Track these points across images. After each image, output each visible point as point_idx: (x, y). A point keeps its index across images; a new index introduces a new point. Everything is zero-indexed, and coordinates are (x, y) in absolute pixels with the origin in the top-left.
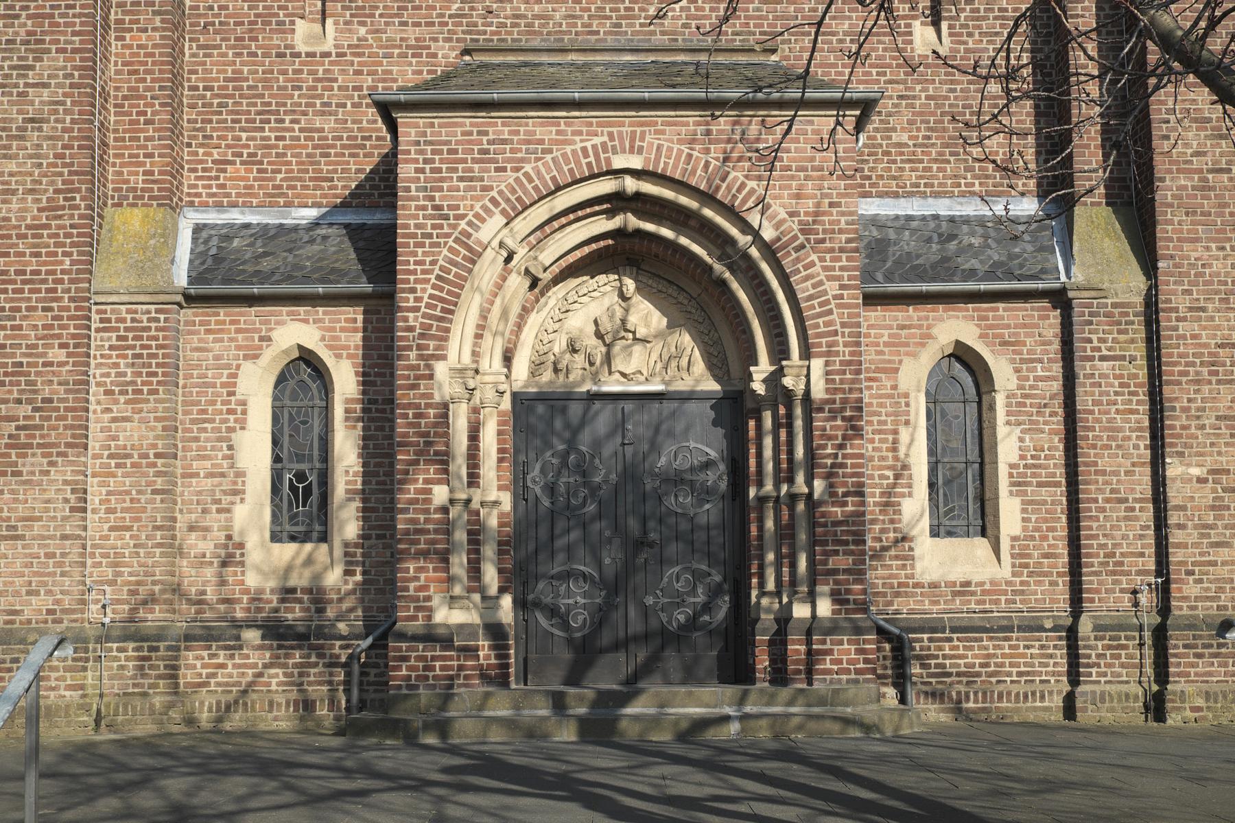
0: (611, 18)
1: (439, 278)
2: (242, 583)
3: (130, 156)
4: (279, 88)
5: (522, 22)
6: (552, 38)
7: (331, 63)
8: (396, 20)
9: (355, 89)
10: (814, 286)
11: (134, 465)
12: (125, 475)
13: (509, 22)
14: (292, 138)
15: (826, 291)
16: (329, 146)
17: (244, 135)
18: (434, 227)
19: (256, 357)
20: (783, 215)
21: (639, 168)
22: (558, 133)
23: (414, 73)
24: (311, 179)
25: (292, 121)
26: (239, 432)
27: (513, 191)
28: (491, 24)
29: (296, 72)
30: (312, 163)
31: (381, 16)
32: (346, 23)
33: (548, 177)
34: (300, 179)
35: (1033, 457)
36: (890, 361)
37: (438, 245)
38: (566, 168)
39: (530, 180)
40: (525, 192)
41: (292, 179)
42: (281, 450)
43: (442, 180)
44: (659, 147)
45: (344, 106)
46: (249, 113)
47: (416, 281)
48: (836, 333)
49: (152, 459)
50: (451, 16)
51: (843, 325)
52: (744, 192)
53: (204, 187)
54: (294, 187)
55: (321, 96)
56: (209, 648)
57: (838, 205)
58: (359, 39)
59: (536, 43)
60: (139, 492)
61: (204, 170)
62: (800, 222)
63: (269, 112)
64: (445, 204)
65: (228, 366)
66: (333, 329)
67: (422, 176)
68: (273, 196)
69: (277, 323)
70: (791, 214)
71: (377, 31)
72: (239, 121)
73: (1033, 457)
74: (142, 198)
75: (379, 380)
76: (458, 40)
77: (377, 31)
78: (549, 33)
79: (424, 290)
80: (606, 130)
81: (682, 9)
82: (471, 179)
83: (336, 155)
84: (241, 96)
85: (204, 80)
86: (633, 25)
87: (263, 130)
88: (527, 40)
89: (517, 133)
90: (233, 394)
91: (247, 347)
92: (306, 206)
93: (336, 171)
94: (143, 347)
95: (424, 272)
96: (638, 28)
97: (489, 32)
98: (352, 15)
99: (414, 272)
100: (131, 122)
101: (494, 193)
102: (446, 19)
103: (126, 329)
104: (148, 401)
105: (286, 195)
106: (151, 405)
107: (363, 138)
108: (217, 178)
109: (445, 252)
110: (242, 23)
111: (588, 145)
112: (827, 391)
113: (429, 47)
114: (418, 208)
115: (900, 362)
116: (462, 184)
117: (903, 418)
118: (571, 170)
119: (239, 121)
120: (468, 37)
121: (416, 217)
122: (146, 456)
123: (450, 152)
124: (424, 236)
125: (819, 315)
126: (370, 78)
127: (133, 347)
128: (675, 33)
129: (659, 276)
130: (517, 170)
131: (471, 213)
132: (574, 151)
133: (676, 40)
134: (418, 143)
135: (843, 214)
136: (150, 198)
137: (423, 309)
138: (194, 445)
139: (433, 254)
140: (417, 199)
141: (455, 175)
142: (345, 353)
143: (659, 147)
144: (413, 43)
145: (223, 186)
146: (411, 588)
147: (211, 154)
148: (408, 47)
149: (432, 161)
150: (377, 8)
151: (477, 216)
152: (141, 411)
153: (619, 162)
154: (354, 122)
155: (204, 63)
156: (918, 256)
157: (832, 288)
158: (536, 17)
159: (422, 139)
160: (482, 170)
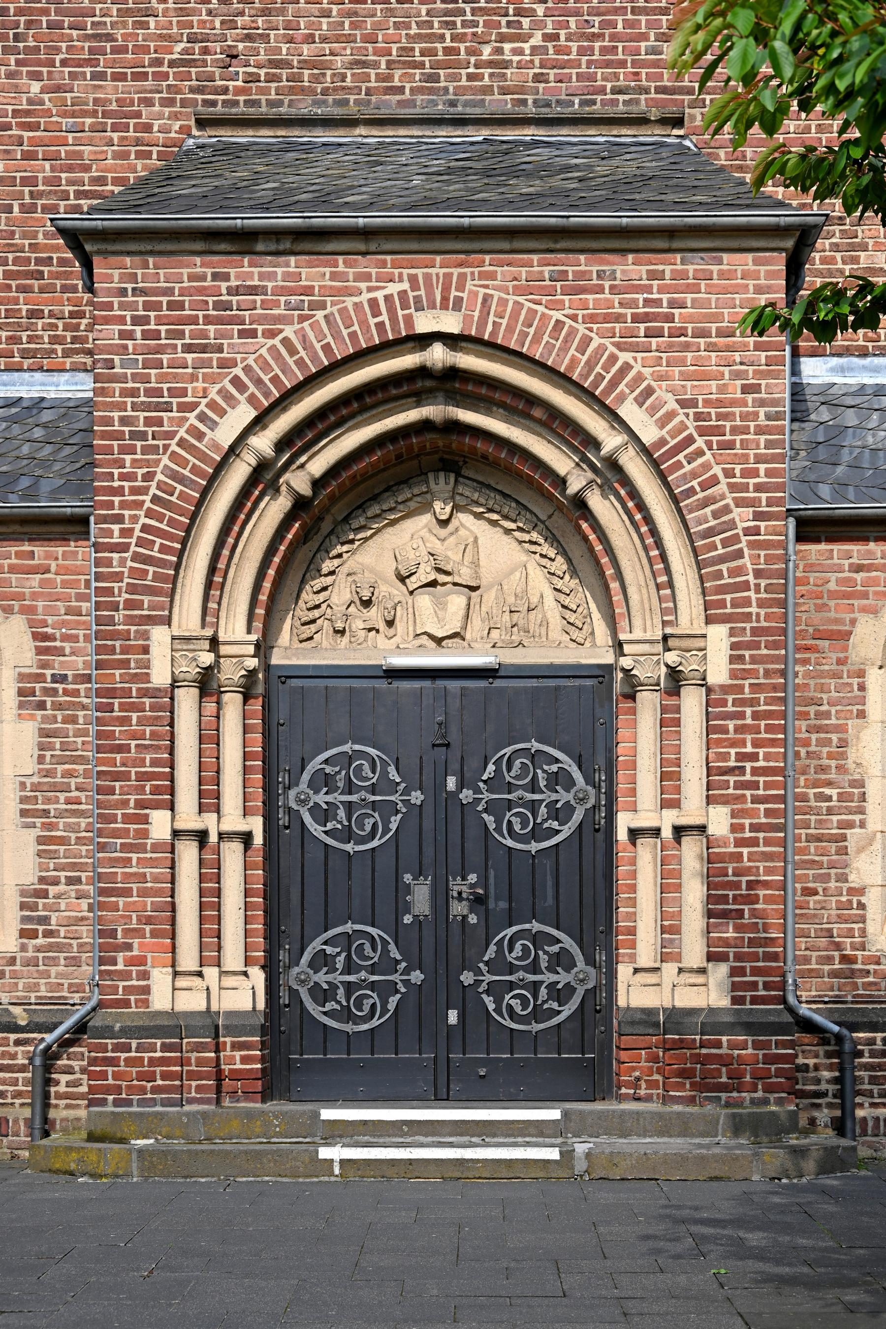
0: (422, 65)
1: (155, 499)
5: (284, 73)
6: (330, 99)
8: (88, 70)
9: (25, 181)
13: (262, 72)
15: (733, 521)
18: (148, 422)
20: (672, 405)
21: (456, 331)
22: (334, 277)
23: (117, 156)
27: (266, 367)
28: (234, 77)
31: (64, 63)
33: (318, 346)
36: (837, 621)
37: (155, 449)
38: (345, 332)
39: (292, 351)
43: (160, 350)
44: (487, 299)
47: (123, 505)
48: (746, 586)
51: (758, 574)
52: (614, 370)
57: (756, 389)
58: (30, 102)
59: (305, 107)
62: (698, 417)
64: (165, 386)
67: (130, 343)
71: (58, 89)
75: (67, 647)
76: (184, 103)
77: (58, 89)
79: (134, 519)
80: (406, 272)
81: (534, 49)
82: (204, 349)
86: (456, 78)
88: (291, 104)
89: (272, 276)
95: (134, 491)
96: (464, 82)
98: (18, 63)
99: (120, 491)
101: (238, 371)
102: (165, 69)
107: (38, 261)
109: (165, 460)
111: (379, 295)
113: (138, 115)
114: (125, 393)
115: (853, 622)
116: (190, 357)
117: (855, 708)
120: (200, 97)
121: (122, 407)
123: (171, 306)
124: (134, 435)
125: (722, 559)
126: (47, 165)
128: (521, 90)
129: (489, 487)
131: (204, 401)
133: (524, 102)
134: (123, 292)
135: (762, 403)
137: (133, 548)
140: (123, 379)
141: (179, 343)
142: (16, 605)
143: (487, 299)
144: (114, 107)
146: (120, 960)
148: (105, 115)
149: (145, 320)
150: (58, 50)
151: (212, 405)
153: (424, 324)
154: (24, 236)
157: (742, 517)
158: (305, 64)
159: (130, 286)
160: (219, 335)
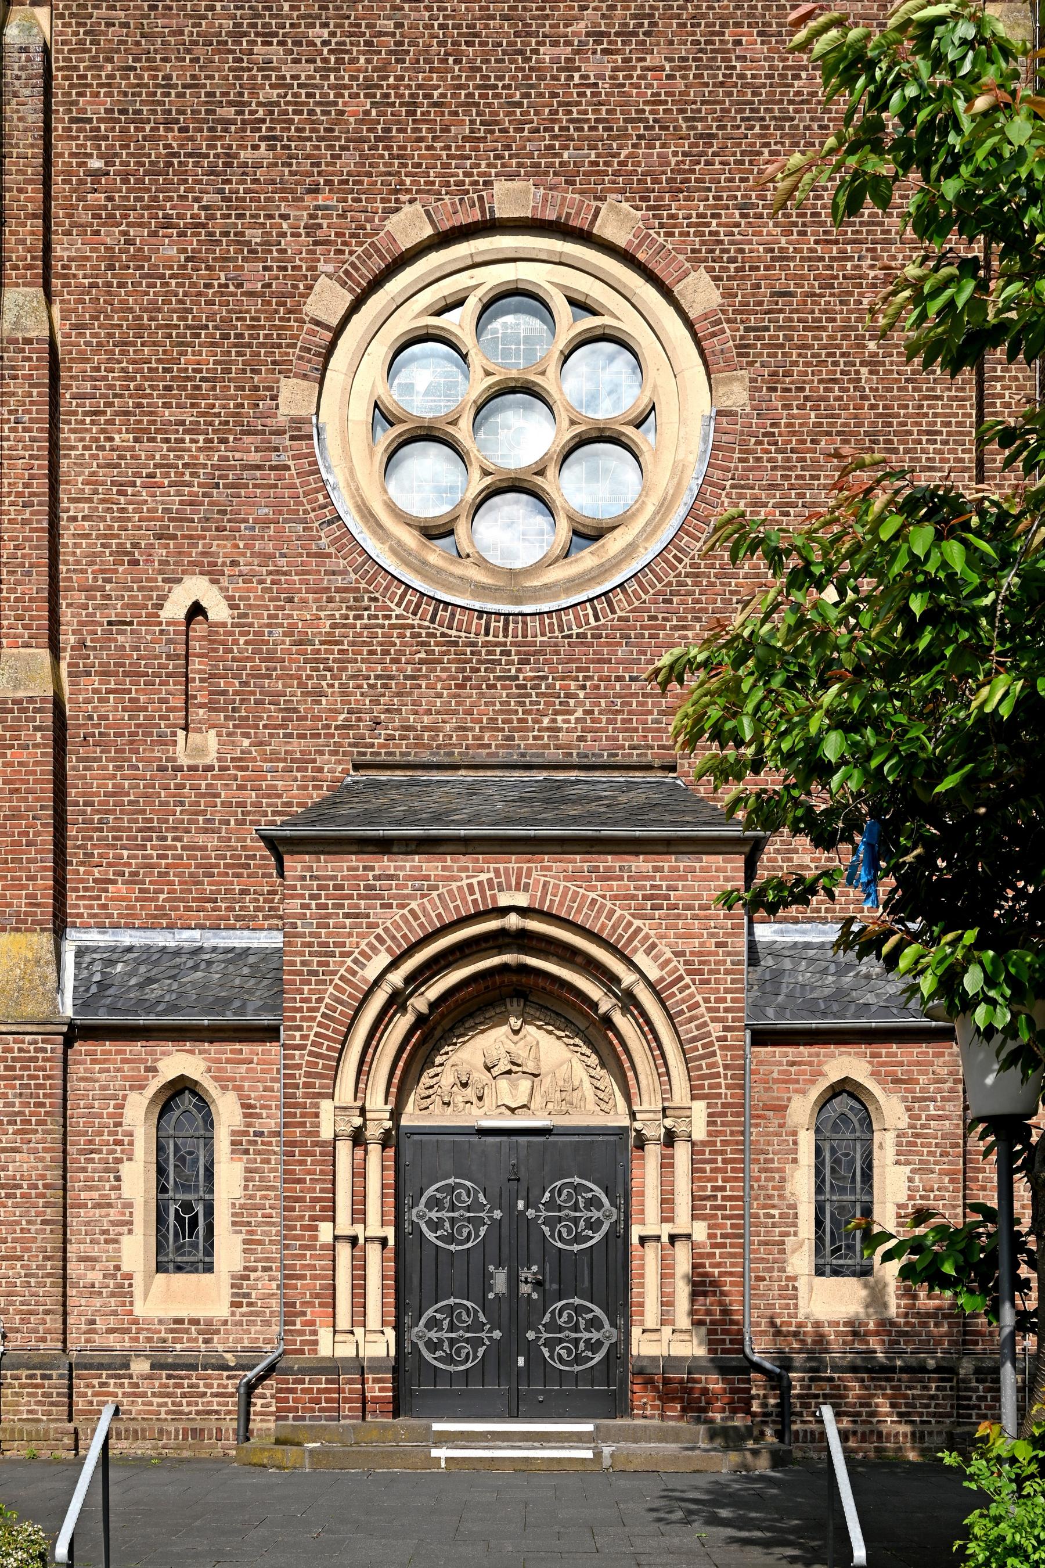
0: (503, 730)
1: (324, 1015)
2: (130, 1313)
3: (13, 879)
4: (161, 804)
5: (412, 734)
7: (214, 777)
9: (239, 804)
10: (698, 1028)
11: (23, 1196)
12: (16, 1206)
14: (174, 857)
16: (212, 866)
17: (125, 853)
19: (142, 1087)
23: (299, 788)
24: (194, 900)
25: (174, 839)
26: (126, 1164)
28: (379, 736)
29: (179, 786)
30: (196, 883)
31: (265, 727)
32: (229, 735)
34: (183, 900)
35: (922, 1197)
36: (778, 1099)
39: (416, 918)
40: (411, 929)
41: (175, 900)
42: (167, 1180)
44: (546, 884)
45: (228, 823)
46: (130, 829)
47: (303, 1019)
48: (718, 1075)
49: (41, 1190)
50: (337, 728)
51: (726, 1067)
53: (86, 907)
54: (177, 909)
55: (203, 813)
56: (100, 1377)
57: (724, 944)
58: (242, 752)
59: (425, 757)
60: (29, 1222)
61: (86, 889)
62: (686, 963)
63: (150, 829)
65: (115, 1097)
66: (219, 1061)
68: (155, 917)
69: (163, 1054)
70: (676, 954)
72: (120, 839)
73: (922, 1197)
74: (25, 922)
76: (345, 754)
77: (261, 744)
78: (438, 747)
79: (310, 1028)
82: (357, 916)
83: (219, 875)
84: (122, 812)
85: (84, 795)
86: (526, 738)
87: (144, 847)
90: (120, 1124)
91: (133, 1078)
92: (189, 928)
93: (219, 892)
94: (30, 1077)
95: (310, 1010)
97: (377, 745)
99: (300, 1010)
100: (13, 843)
101: (380, 931)
103: (14, 1059)
104: (36, 1132)
105: (169, 916)
106: (40, 1136)
107: (247, 857)
108: (99, 898)
109: (331, 989)
110: (122, 735)
111: (474, 881)
112: (710, 1134)
113: (314, 761)
114: (305, 945)
115: (789, 1099)
116: (348, 921)
118: (456, 908)
119: (120, 839)
121: (302, 954)
122: (36, 1187)
123: (335, 887)
124: (311, 973)
125: (702, 1057)
127: (21, 1077)
130: (402, 906)
132: (459, 888)
134: (303, 878)
136: (33, 922)
138: (82, 1176)
139: (319, 991)
143: (546, 884)
145: (104, 907)
147: (92, 873)
149: (319, 896)
151: (363, 953)
152: (29, 1141)
153: (504, 900)
154: (238, 840)
155: (84, 777)
156: (813, 989)
157: (715, 1030)
158: (425, 729)
